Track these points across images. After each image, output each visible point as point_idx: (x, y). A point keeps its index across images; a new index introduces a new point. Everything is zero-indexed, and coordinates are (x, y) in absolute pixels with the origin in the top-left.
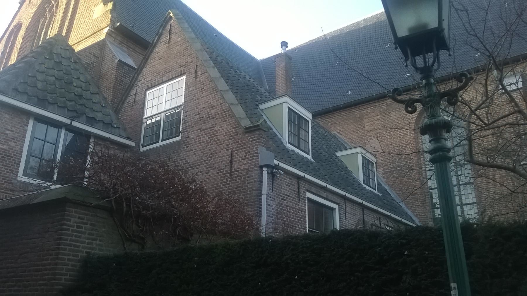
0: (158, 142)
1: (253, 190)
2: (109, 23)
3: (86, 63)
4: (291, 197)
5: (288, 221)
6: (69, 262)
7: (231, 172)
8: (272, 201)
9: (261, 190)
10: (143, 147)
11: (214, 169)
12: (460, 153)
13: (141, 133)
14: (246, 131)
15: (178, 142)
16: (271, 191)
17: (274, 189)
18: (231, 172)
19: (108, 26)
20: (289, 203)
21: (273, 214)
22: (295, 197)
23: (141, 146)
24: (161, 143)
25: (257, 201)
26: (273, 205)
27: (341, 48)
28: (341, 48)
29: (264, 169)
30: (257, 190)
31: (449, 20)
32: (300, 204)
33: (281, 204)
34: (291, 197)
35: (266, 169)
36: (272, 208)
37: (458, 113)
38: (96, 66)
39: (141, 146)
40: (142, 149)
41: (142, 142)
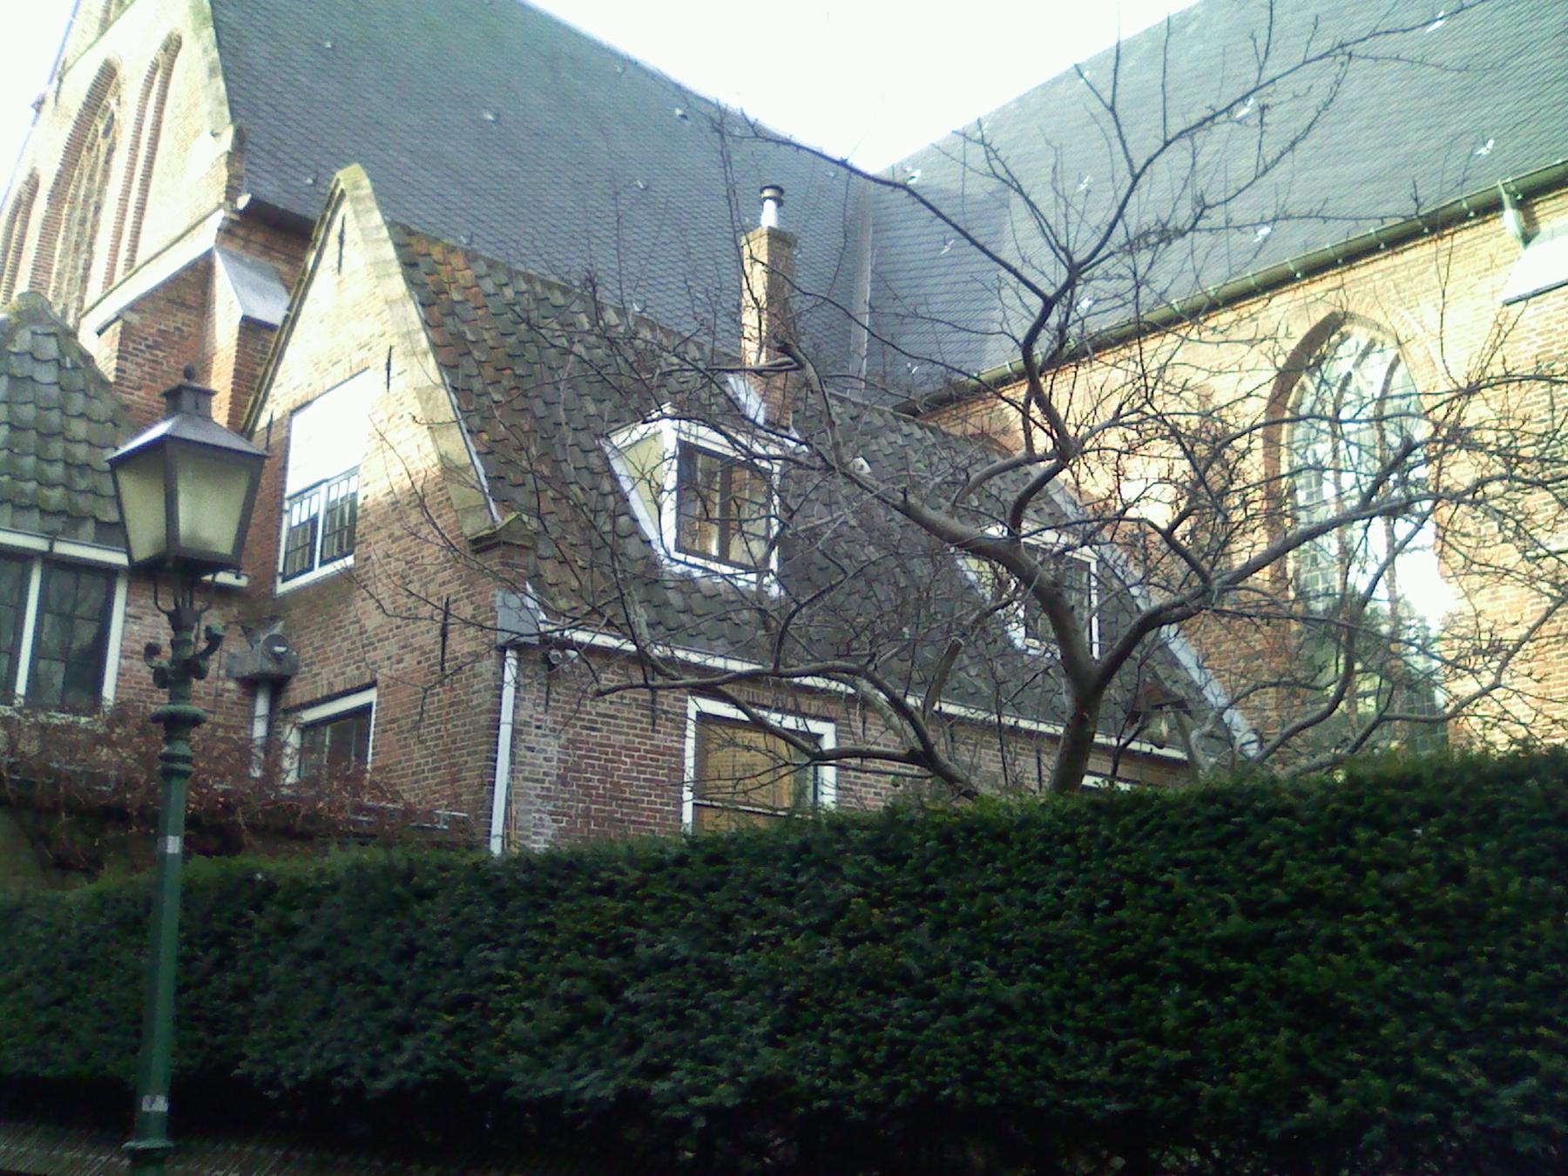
0: (311, 569)
1: (481, 713)
2: (222, 200)
3: (159, 330)
4: (622, 718)
5: (604, 788)
6: (353, 817)
7: (443, 661)
8: (544, 736)
9: (499, 712)
10: (283, 581)
11: (412, 652)
12: (622, 697)
13: (278, 542)
14: (475, 547)
15: (348, 570)
16: (541, 709)
17: (551, 703)
18: (443, 661)
19: (220, 206)
20: (612, 737)
21: (545, 774)
22: (639, 717)
23: (279, 580)
24: (319, 572)
25: (487, 743)
26: (549, 749)
27: (957, 264)
28: (957, 264)
29: (508, 653)
30: (489, 711)
31: (141, 210)
32: (661, 736)
33: (582, 742)
34: (622, 718)
35: (514, 654)
36: (542, 756)
37: (1094, 479)
38: (191, 334)
39: (279, 580)
40: (282, 588)
41: (281, 569)
